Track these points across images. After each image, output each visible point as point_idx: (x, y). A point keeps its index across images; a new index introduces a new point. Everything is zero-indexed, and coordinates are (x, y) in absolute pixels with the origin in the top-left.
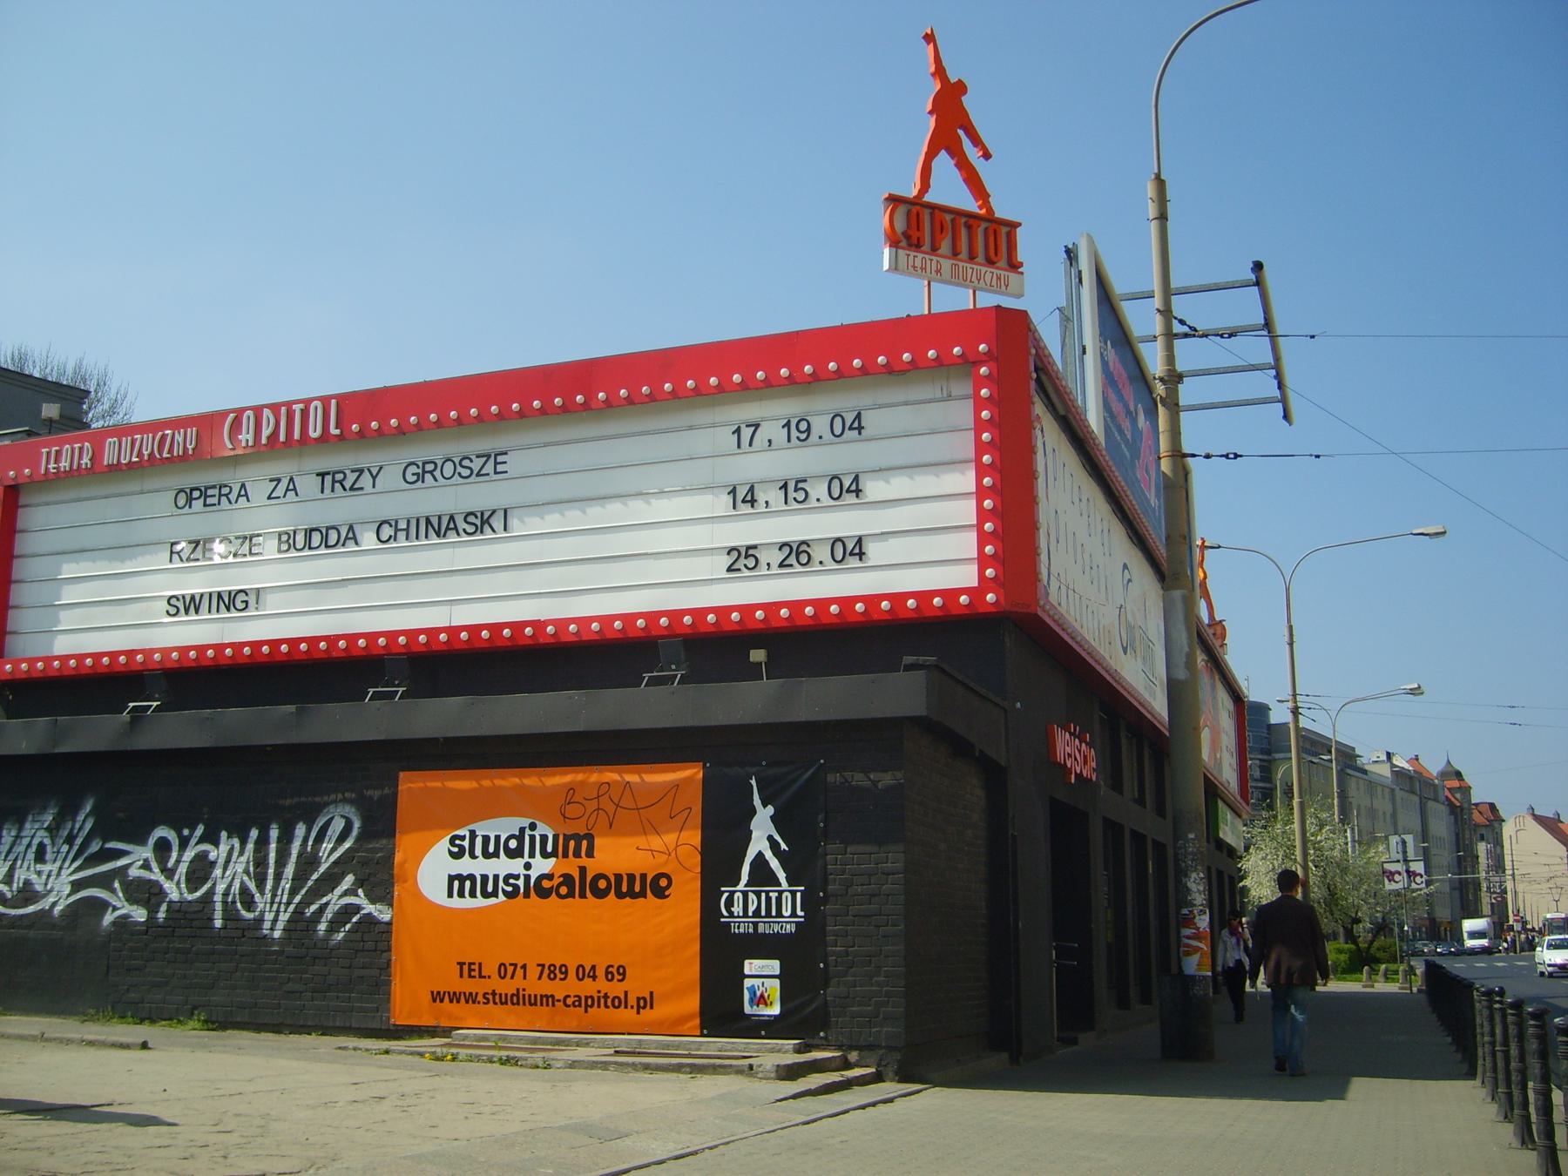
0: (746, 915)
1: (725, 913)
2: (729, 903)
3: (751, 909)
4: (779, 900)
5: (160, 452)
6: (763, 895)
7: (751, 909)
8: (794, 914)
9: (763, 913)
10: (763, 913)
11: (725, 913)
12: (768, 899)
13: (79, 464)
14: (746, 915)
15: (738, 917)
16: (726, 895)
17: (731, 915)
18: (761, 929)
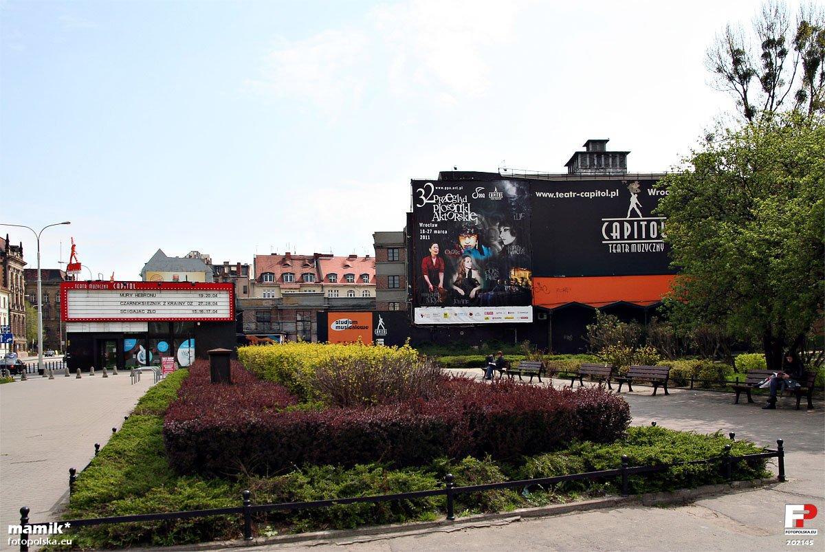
0: (622, 237)
1: (606, 238)
2: (609, 230)
3: (626, 234)
4: (648, 227)
5: (652, 250)
6: (636, 223)
7: (626, 234)
8: (659, 237)
9: (636, 237)
10: (636, 237)
11: (606, 238)
12: (640, 227)
13: (612, 251)
14: (622, 237)
15: (616, 240)
16: (606, 224)
17: (611, 238)
18: (633, 250)
